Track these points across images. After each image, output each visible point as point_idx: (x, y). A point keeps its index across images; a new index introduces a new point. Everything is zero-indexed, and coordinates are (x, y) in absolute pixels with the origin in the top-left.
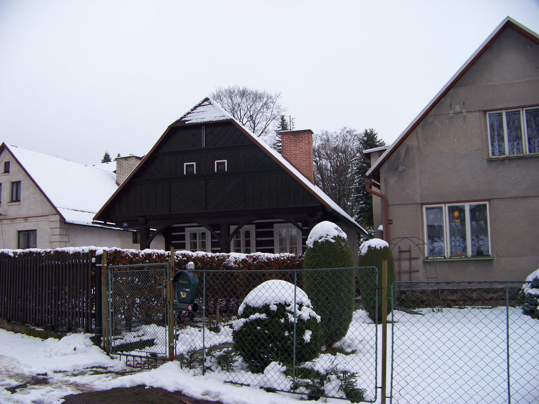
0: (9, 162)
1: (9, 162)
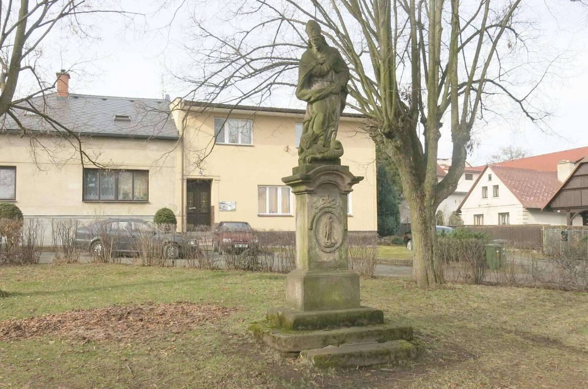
0: (491, 175)
1: (491, 175)
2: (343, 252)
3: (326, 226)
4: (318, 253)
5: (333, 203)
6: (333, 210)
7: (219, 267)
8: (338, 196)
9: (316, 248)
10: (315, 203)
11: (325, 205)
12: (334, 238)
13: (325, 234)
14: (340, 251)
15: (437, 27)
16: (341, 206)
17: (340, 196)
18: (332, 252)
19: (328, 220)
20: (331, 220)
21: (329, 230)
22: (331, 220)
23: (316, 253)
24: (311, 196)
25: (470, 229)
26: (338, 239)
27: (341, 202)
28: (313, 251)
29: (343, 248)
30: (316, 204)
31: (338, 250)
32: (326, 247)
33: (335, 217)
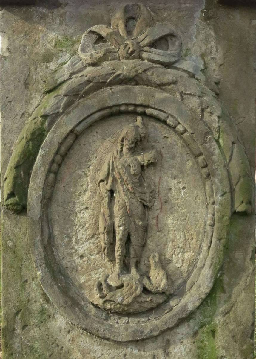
2: (220, 340)
3: (112, 192)
4: (65, 340)
5: (156, 54)
6: (159, 95)
7: (162, 168)
8: (198, 14)
9: (51, 317)
10: (48, 58)
11: (107, 66)
12: (163, 264)
13: (102, 240)
14: (203, 335)
15: (63, 149)
16: (215, 72)
17: (207, 18)
18: (152, 338)
19: (128, 158)
20: (144, 158)
21: (128, 215)
22: (144, 158)
23: (55, 343)
24: (28, 19)
25: (141, 221)
26: (193, 264)
27: (219, 56)
28: (35, 332)
29: (219, 320)
30: (52, 66)
31: (184, 329)
32: (109, 312)
33: (173, 138)
